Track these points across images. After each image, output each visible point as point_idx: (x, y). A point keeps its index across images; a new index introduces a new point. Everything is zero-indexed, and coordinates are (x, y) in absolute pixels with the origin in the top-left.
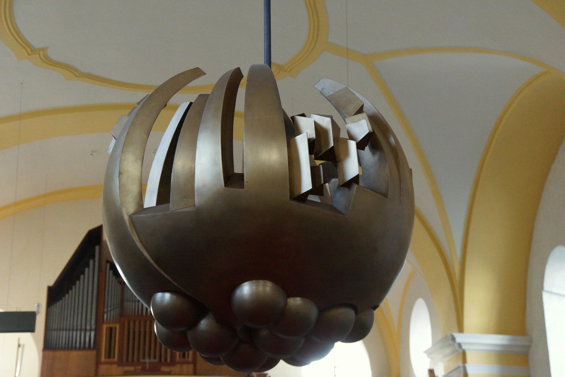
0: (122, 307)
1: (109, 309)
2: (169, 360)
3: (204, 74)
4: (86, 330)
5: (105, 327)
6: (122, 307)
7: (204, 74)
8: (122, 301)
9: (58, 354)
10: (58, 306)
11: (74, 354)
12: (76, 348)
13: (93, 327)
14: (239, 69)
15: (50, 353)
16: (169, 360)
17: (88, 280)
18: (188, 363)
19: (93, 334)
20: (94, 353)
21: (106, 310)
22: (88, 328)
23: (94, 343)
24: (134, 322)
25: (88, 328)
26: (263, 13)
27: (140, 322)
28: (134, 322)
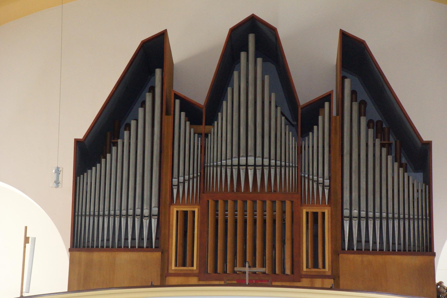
0: (203, 177)
1: (181, 179)
2: (288, 272)
3: (341, 30)
4: (142, 216)
5: (174, 210)
6: (203, 177)
7: (341, 30)
8: (204, 168)
9: (96, 256)
10: (92, 175)
11: (124, 257)
12: (126, 247)
13: (155, 210)
14: (75, 139)
15: (83, 255)
16: (288, 272)
17: (145, 121)
18: (323, 276)
19: (154, 222)
20: (158, 255)
21: (175, 181)
22: (146, 212)
23: (157, 238)
24: (226, 202)
25: (146, 212)
26: (178, 92)
27: (235, 202)
28: (226, 202)
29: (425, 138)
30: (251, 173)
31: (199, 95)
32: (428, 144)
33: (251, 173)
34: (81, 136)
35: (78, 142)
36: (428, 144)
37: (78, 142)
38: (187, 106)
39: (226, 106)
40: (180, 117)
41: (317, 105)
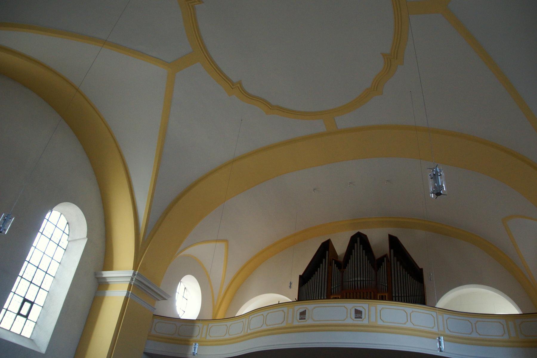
25: (400, 295)
29: (420, 267)
30: (359, 283)
31: (341, 259)
32: (422, 270)
33: (359, 283)
34: (301, 274)
35: (300, 276)
36: (422, 270)
37: (300, 276)
38: (338, 264)
39: (350, 261)
40: (334, 266)
41: (382, 259)
